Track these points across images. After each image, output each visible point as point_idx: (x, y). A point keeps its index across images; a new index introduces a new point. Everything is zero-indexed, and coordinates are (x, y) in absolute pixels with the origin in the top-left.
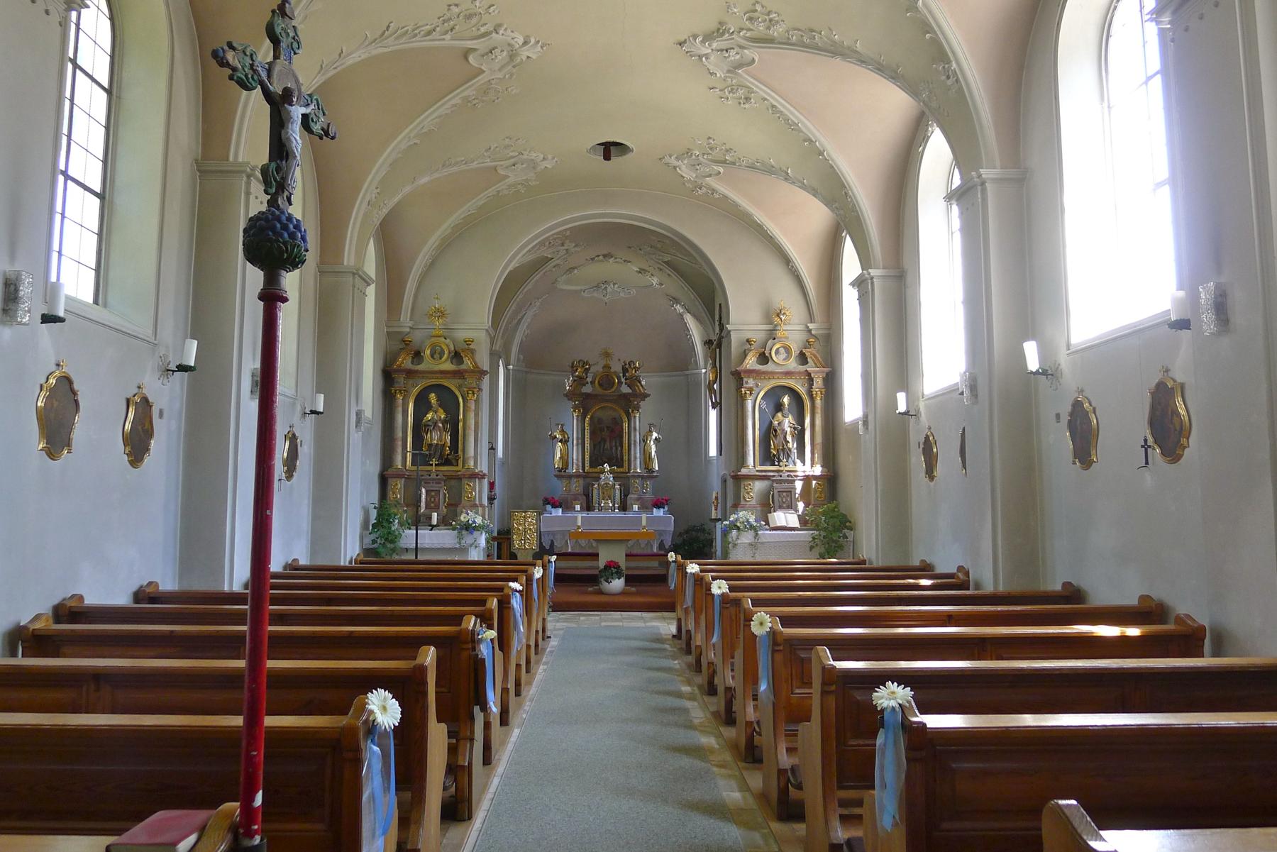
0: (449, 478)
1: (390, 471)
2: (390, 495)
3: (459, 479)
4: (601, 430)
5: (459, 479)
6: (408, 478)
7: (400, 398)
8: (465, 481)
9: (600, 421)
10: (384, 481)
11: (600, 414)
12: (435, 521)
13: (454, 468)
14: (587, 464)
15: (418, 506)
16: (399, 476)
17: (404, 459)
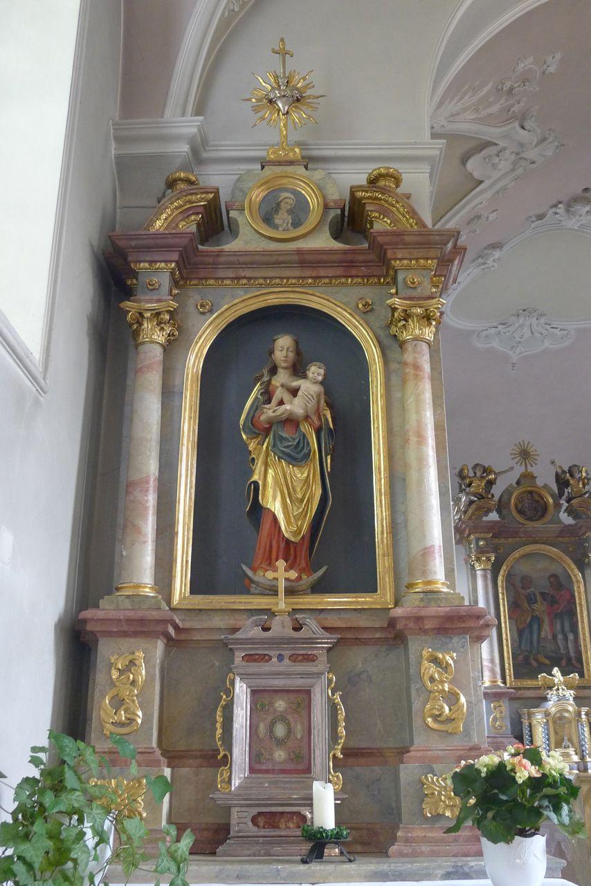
0: (346, 638)
1: (107, 608)
2: (104, 711)
3: (394, 635)
4: (531, 600)
5: (394, 635)
6: (178, 642)
7: (154, 335)
8: (421, 648)
9: (526, 581)
10: (79, 649)
11: (525, 568)
12: (325, 815)
13: (364, 600)
14: (509, 671)
15: (218, 760)
16: (139, 627)
17: (160, 561)
